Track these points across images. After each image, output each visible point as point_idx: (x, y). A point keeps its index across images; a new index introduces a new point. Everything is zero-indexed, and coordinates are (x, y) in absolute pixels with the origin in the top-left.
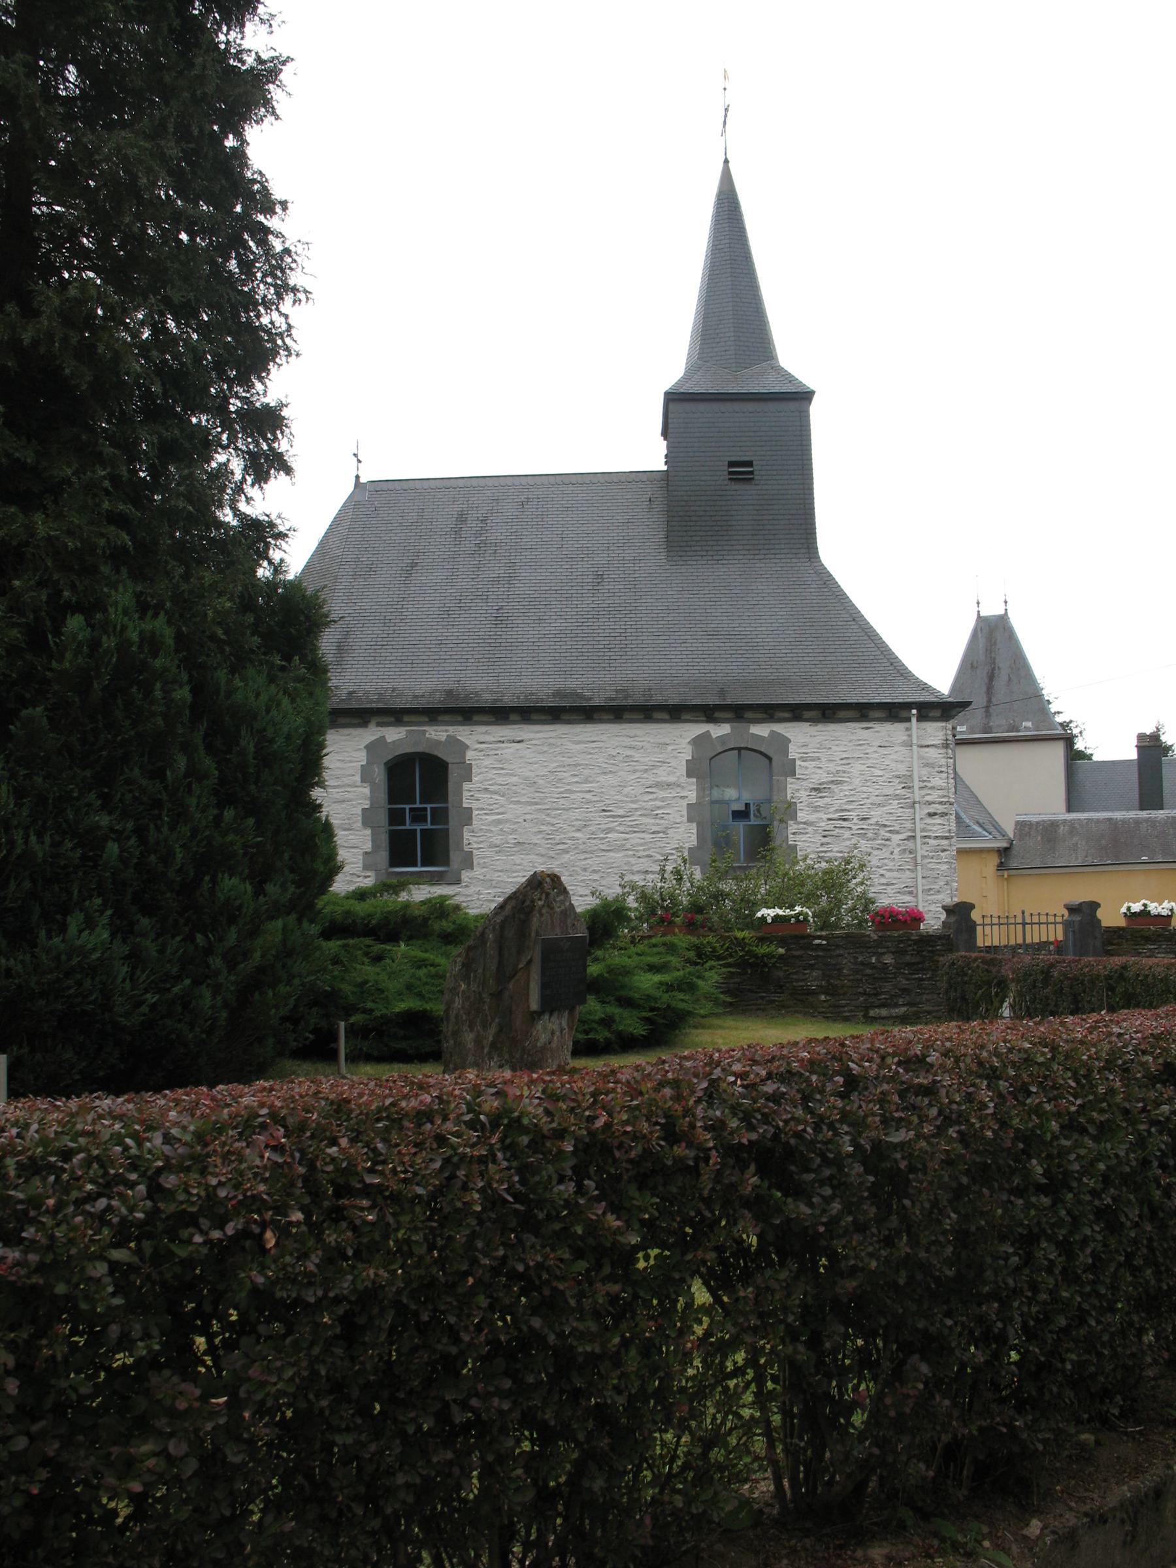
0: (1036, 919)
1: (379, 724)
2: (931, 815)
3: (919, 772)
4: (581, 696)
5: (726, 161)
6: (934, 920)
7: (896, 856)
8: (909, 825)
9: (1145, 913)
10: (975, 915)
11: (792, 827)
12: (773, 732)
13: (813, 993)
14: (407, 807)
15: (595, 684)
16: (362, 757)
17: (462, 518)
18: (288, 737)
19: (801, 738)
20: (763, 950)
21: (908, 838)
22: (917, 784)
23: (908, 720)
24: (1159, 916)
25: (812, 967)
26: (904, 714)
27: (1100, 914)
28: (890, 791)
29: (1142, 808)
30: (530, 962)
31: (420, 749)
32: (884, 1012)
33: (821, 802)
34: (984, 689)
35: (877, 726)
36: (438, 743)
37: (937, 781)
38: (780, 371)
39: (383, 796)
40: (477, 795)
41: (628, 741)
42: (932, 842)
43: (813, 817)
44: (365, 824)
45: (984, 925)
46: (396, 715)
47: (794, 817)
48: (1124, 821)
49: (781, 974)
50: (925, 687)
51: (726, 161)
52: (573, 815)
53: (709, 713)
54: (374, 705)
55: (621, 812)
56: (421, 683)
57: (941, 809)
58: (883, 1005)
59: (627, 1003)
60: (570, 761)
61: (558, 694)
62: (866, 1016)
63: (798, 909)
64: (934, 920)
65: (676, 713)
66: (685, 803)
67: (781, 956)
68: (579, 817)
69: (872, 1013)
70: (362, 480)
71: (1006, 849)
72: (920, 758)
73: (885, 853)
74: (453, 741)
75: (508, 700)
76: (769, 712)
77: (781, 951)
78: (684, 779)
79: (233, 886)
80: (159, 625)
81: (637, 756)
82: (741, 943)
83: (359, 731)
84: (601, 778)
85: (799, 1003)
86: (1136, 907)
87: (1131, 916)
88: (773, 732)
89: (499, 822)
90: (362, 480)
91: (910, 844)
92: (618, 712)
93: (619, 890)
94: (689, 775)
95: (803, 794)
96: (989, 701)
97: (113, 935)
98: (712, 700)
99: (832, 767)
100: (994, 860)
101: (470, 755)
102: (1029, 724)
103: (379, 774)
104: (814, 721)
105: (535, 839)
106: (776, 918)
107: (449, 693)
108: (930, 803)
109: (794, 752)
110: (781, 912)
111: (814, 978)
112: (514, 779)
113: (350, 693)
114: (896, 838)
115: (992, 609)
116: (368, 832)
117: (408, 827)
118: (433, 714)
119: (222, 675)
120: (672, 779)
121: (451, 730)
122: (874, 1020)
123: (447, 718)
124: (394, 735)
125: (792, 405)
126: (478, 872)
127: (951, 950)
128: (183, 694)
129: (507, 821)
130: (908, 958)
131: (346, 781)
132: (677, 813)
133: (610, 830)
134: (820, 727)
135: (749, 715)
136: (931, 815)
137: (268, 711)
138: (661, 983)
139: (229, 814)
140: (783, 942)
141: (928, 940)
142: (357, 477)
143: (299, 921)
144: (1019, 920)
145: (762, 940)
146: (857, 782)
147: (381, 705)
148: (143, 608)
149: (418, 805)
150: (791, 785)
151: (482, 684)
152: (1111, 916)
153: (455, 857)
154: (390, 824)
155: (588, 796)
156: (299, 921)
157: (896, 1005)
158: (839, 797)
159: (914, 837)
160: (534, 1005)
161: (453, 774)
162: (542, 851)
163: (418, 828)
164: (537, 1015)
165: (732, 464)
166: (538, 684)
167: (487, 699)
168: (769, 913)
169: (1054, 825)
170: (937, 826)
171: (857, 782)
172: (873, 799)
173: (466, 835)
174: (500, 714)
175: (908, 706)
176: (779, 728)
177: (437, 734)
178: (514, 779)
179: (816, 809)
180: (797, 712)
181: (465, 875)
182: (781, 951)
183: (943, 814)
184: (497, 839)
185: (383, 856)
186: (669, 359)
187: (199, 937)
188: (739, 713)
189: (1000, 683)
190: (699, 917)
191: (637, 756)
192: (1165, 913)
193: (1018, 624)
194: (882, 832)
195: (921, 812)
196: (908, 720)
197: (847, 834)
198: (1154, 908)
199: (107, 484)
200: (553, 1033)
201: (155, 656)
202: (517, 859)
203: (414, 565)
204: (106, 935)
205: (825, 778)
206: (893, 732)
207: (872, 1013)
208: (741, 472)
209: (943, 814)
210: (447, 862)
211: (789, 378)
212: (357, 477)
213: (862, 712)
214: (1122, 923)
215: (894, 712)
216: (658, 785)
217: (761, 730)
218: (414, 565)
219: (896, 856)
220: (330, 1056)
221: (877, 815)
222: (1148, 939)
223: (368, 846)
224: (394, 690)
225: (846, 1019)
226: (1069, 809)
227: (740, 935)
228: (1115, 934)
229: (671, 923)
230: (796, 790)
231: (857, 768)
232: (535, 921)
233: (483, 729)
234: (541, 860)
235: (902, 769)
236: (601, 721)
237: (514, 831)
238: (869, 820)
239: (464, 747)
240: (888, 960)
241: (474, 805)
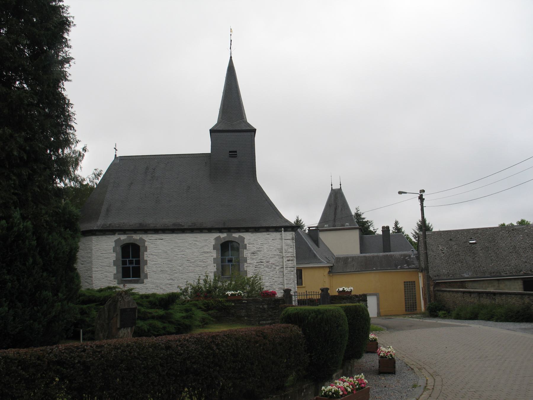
0: (310, 293)
1: (119, 234)
2: (288, 260)
3: (285, 247)
4: (181, 225)
5: (231, 57)
6: (280, 294)
7: (278, 273)
8: (281, 264)
9: (343, 291)
10: (292, 293)
11: (246, 265)
12: (239, 236)
13: (243, 317)
14: (128, 260)
15: (185, 222)
16: (113, 244)
17: (147, 168)
18: (63, 252)
19: (248, 238)
20: (227, 304)
21: (282, 268)
22: (284, 251)
23: (281, 231)
24: (348, 292)
25: (242, 309)
26: (280, 230)
27: (329, 291)
28: (275, 253)
29: (384, 252)
30: (117, 315)
31: (131, 242)
32: (264, 322)
33: (254, 257)
34: (333, 213)
35: (271, 233)
36: (137, 240)
37: (290, 250)
38: (246, 122)
39: (120, 256)
40: (149, 256)
41: (195, 239)
42: (289, 269)
43: (252, 262)
44: (114, 265)
45: (295, 295)
46: (123, 231)
47: (246, 261)
48: (369, 257)
49: (233, 311)
50: (287, 221)
51: (231, 57)
52: (178, 262)
53: (220, 230)
54: (117, 228)
55: (193, 261)
56: (134, 221)
57: (291, 258)
58: (264, 320)
59: (171, 322)
60: (177, 245)
61: (174, 225)
62: (259, 323)
63: (239, 291)
64: (280, 294)
65: (210, 230)
66: (213, 258)
67: (233, 306)
68: (178, 264)
69: (261, 322)
70: (117, 156)
71: (331, 267)
72: (285, 243)
73: (274, 272)
74: (141, 239)
75: (158, 227)
76: (239, 230)
77: (233, 304)
78: (212, 251)
79: (48, 294)
80: (29, 224)
81: (198, 243)
82: (221, 302)
83: (112, 236)
84: (187, 250)
85: (239, 319)
86: (341, 289)
87: (339, 292)
88: (239, 236)
89: (155, 264)
90: (117, 156)
91: (282, 270)
92: (192, 230)
93: (186, 286)
94: (214, 249)
95: (249, 255)
96: (335, 217)
97: (9, 309)
98: (221, 226)
99: (258, 246)
100: (327, 270)
101: (146, 244)
102: (348, 224)
103: (119, 250)
104: (252, 232)
105: (167, 269)
106: (232, 295)
107: (140, 224)
108: (288, 257)
109: (246, 242)
110: (233, 293)
111: (243, 313)
112: (160, 251)
113: (110, 224)
114: (277, 268)
115: (336, 187)
116: (115, 267)
117: (128, 266)
118: (135, 231)
119: (45, 235)
120: (208, 250)
121: (141, 236)
122: (262, 324)
123: (139, 232)
124: (123, 237)
125: (249, 134)
126: (149, 279)
127: (284, 303)
128: (34, 243)
129: (158, 264)
130: (271, 306)
131: (108, 251)
132: (211, 261)
133: (190, 266)
134: (254, 234)
135: (232, 231)
136: (288, 260)
137: (58, 245)
138: (182, 316)
139: (45, 274)
140: (233, 301)
141: (278, 300)
142: (116, 155)
143: (68, 303)
144: (305, 294)
145: (227, 301)
146: (265, 251)
147: (119, 228)
148: (24, 218)
149: (131, 259)
150: (245, 252)
151: (150, 222)
152: (333, 292)
153: (142, 275)
154: (123, 265)
155: (183, 256)
156: (68, 303)
157: (268, 320)
158: (260, 256)
159: (283, 267)
160: (118, 326)
161: (142, 249)
162: (169, 273)
163: (131, 266)
164: (120, 329)
165: (230, 152)
166: (167, 221)
167: (152, 226)
168: (229, 293)
169: (359, 256)
170: (290, 264)
171: (265, 251)
172: (271, 256)
173: (145, 268)
174: (156, 231)
175: (281, 227)
176: (242, 234)
177: (136, 237)
178: (160, 251)
179: (253, 259)
180: (247, 230)
181: (145, 281)
182: (233, 304)
183: (292, 260)
184: (155, 269)
185: (120, 275)
186: (213, 120)
187: (35, 308)
188: (229, 230)
189: (339, 209)
190: (208, 295)
191: (198, 243)
192: (349, 291)
193: (344, 191)
194: (274, 266)
195: (285, 260)
196: (281, 231)
197: (262, 267)
198: (346, 289)
199: (13, 185)
200: (125, 334)
201: (27, 233)
202: (161, 275)
203: (132, 183)
204: (7, 309)
205: (256, 249)
206: (276, 235)
207: (261, 322)
208: (233, 154)
209: (292, 260)
210: (139, 276)
211: (249, 125)
212: (116, 155)
213: (267, 229)
214: (337, 294)
215: (277, 229)
216: (204, 252)
217: (236, 235)
218: (132, 183)
219: (278, 273)
220: (78, 339)
221: (272, 261)
222: (344, 299)
223: (115, 272)
224: (124, 223)
225: (253, 325)
226: (361, 253)
227: (220, 300)
228: (334, 297)
229: (200, 296)
230: (246, 253)
231: (266, 246)
232: (119, 304)
233: (150, 235)
234: (168, 276)
235: (279, 247)
236: (187, 233)
237: (160, 267)
238: (268, 263)
239: (144, 241)
240: (266, 306)
241: (148, 259)
